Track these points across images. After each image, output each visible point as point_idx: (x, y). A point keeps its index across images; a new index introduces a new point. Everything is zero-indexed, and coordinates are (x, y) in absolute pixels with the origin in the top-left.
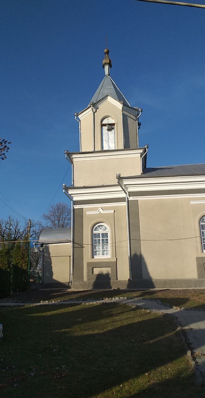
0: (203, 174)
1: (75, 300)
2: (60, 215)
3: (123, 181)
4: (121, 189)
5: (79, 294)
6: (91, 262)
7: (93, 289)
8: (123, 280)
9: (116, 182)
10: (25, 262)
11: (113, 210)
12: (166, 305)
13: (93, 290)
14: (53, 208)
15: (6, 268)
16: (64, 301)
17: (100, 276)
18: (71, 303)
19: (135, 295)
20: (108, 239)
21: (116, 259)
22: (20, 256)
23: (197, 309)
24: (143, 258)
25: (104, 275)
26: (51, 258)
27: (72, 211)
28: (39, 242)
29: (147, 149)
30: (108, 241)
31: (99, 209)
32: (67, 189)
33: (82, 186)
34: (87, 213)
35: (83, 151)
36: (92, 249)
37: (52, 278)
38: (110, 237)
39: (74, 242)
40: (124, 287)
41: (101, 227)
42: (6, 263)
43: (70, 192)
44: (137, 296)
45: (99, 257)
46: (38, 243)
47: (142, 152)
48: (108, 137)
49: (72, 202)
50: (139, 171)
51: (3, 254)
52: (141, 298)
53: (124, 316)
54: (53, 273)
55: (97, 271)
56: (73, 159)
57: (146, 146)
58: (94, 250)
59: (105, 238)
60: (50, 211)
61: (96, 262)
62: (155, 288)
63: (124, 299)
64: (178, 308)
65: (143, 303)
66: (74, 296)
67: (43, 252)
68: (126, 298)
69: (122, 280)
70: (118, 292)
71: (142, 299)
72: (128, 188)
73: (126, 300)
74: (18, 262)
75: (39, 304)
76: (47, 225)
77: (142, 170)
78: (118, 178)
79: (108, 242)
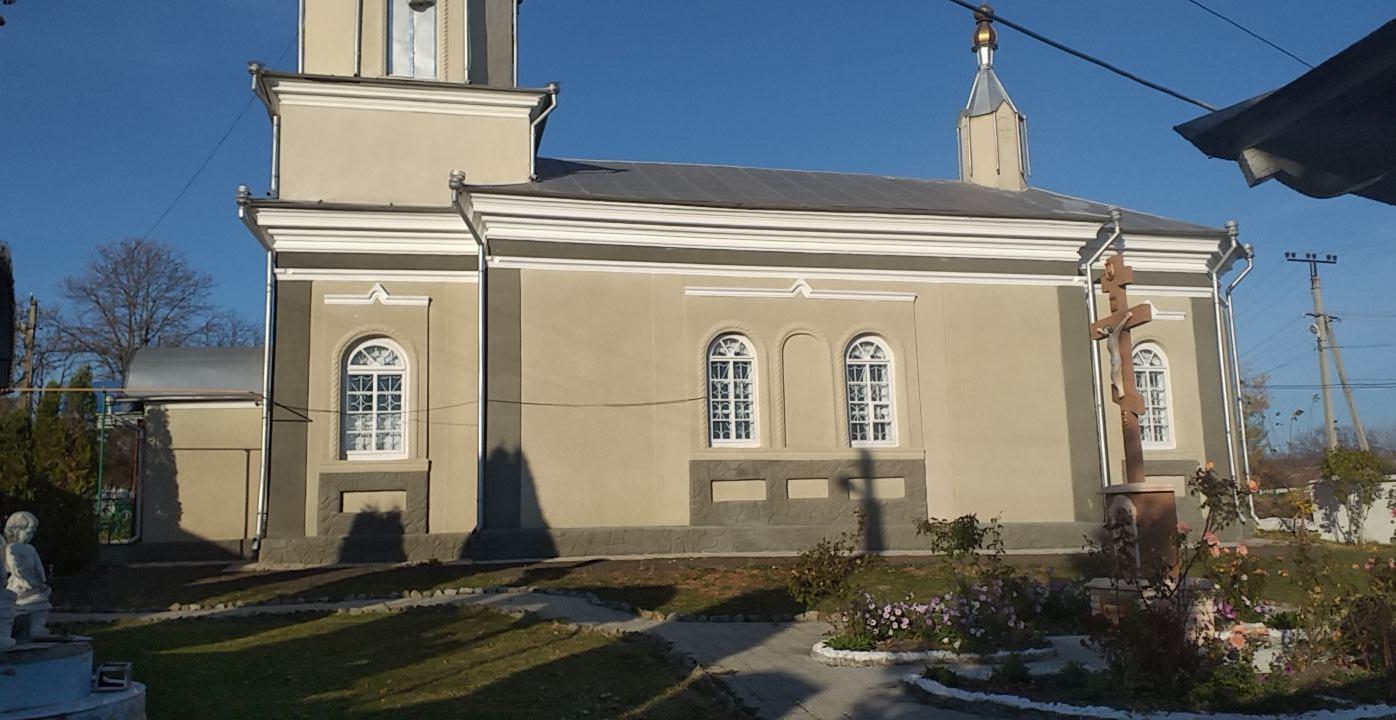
0: (728, 204)
1: (301, 600)
2: (138, 282)
3: (473, 200)
4: (465, 227)
5: (290, 588)
6: (337, 474)
7: (340, 562)
8: (447, 534)
9: (447, 198)
10: (79, 466)
11: (427, 298)
12: (619, 609)
13: (340, 566)
14: (107, 256)
15: (21, 487)
16: (260, 603)
17: (367, 521)
18: (297, 612)
19: (507, 580)
20: (400, 396)
21: (427, 465)
22: (58, 443)
23: (711, 618)
24: (526, 463)
25: (382, 515)
26: (176, 453)
27: (269, 288)
28: (127, 393)
29: (554, 96)
30: (400, 400)
31: (374, 289)
32: (253, 205)
33: (314, 199)
34: (326, 301)
35: (310, 71)
36: (341, 424)
37: (177, 525)
38: (408, 390)
39: (275, 400)
40: (450, 558)
41: (376, 354)
42: (22, 468)
43: (265, 218)
44: (514, 581)
45: (362, 457)
46: (122, 397)
47: (536, 104)
48: (411, 32)
49: (269, 254)
50: (522, 171)
51: (8, 436)
52: (531, 589)
53: (501, 644)
54: (183, 506)
55: (355, 503)
56: (281, 96)
57: (552, 87)
58: (349, 432)
59: (390, 392)
60: (94, 268)
61: (356, 473)
62: (557, 557)
63: (473, 592)
64: (659, 617)
65: (545, 605)
66: (290, 588)
67: (141, 433)
68: (479, 591)
69: (444, 532)
70: (433, 574)
71: (535, 591)
72: (488, 225)
73: (479, 598)
74: (51, 464)
75: (164, 616)
76: (81, 322)
77: (535, 167)
78: (456, 188)
79: (399, 407)
